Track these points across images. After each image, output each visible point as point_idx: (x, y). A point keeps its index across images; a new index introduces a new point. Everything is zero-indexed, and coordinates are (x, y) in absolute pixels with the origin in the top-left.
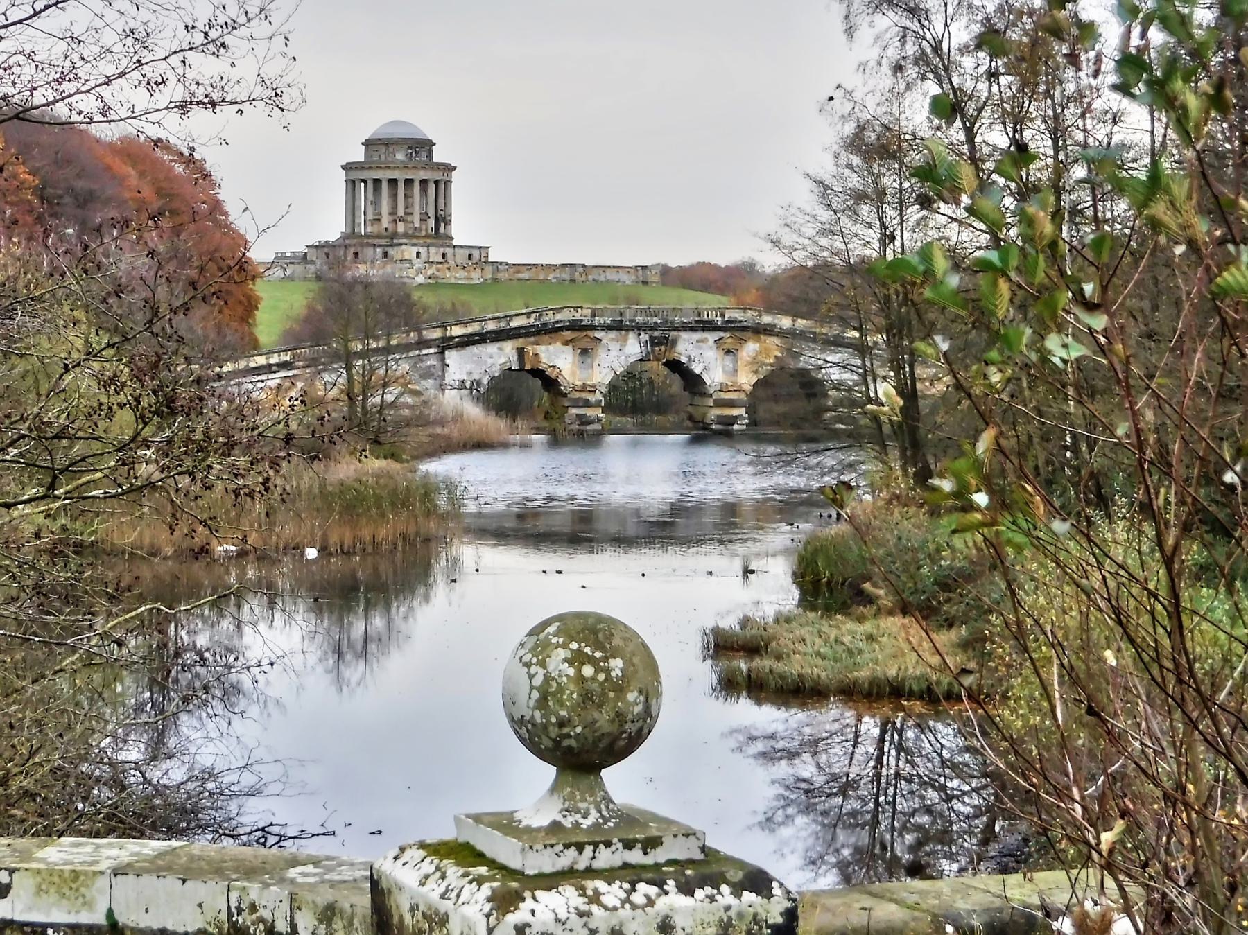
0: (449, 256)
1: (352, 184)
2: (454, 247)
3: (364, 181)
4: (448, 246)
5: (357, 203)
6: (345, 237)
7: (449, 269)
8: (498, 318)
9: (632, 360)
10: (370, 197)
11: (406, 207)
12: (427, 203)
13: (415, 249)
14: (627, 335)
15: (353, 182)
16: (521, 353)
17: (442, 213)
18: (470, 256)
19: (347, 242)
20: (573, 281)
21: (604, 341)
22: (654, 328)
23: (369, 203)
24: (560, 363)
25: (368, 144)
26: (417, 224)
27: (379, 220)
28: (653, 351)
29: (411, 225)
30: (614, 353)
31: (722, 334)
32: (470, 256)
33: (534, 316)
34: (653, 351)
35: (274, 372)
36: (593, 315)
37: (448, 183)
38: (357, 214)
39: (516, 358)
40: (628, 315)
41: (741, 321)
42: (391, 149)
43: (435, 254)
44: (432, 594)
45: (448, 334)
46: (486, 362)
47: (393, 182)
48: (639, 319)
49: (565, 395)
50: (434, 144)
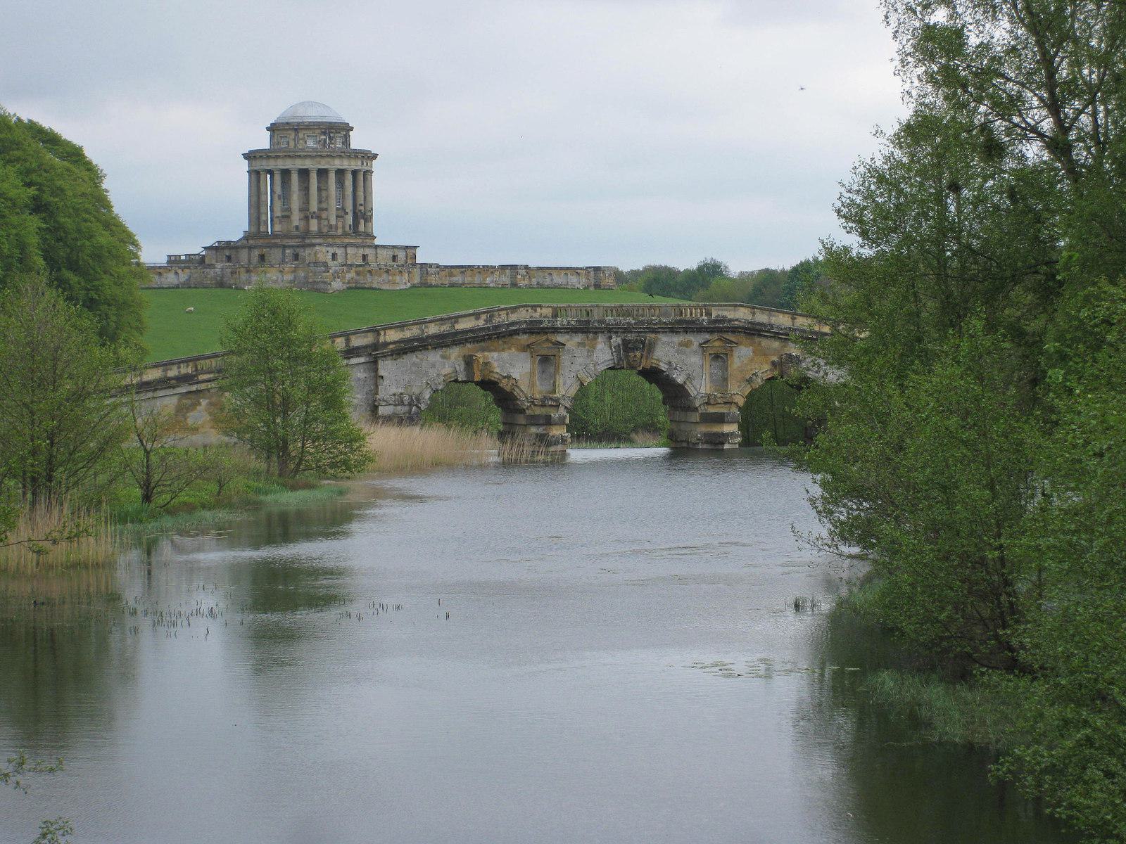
0: (371, 258)
1: (255, 175)
2: (376, 247)
3: (271, 172)
4: (369, 246)
5: (263, 197)
6: (247, 236)
7: (370, 272)
8: (442, 319)
9: (602, 368)
10: (278, 189)
11: (320, 202)
12: (344, 198)
13: (331, 250)
14: (595, 339)
15: (258, 173)
16: (469, 362)
17: (362, 208)
18: (394, 258)
19: (251, 242)
20: (514, 285)
21: (568, 345)
22: (627, 329)
23: (276, 198)
24: (516, 374)
25: (273, 129)
26: (333, 222)
27: (288, 217)
28: (627, 357)
29: (326, 223)
30: (579, 360)
31: (708, 336)
32: (394, 258)
33: (484, 317)
34: (627, 357)
35: (174, 387)
36: (555, 316)
37: (368, 173)
38: (262, 210)
39: (463, 367)
40: (596, 315)
41: (730, 321)
42: (301, 135)
43: (354, 255)
44: (330, 564)
45: (382, 339)
46: (427, 373)
47: (304, 173)
48: (609, 319)
49: (522, 411)
50: (352, 129)
